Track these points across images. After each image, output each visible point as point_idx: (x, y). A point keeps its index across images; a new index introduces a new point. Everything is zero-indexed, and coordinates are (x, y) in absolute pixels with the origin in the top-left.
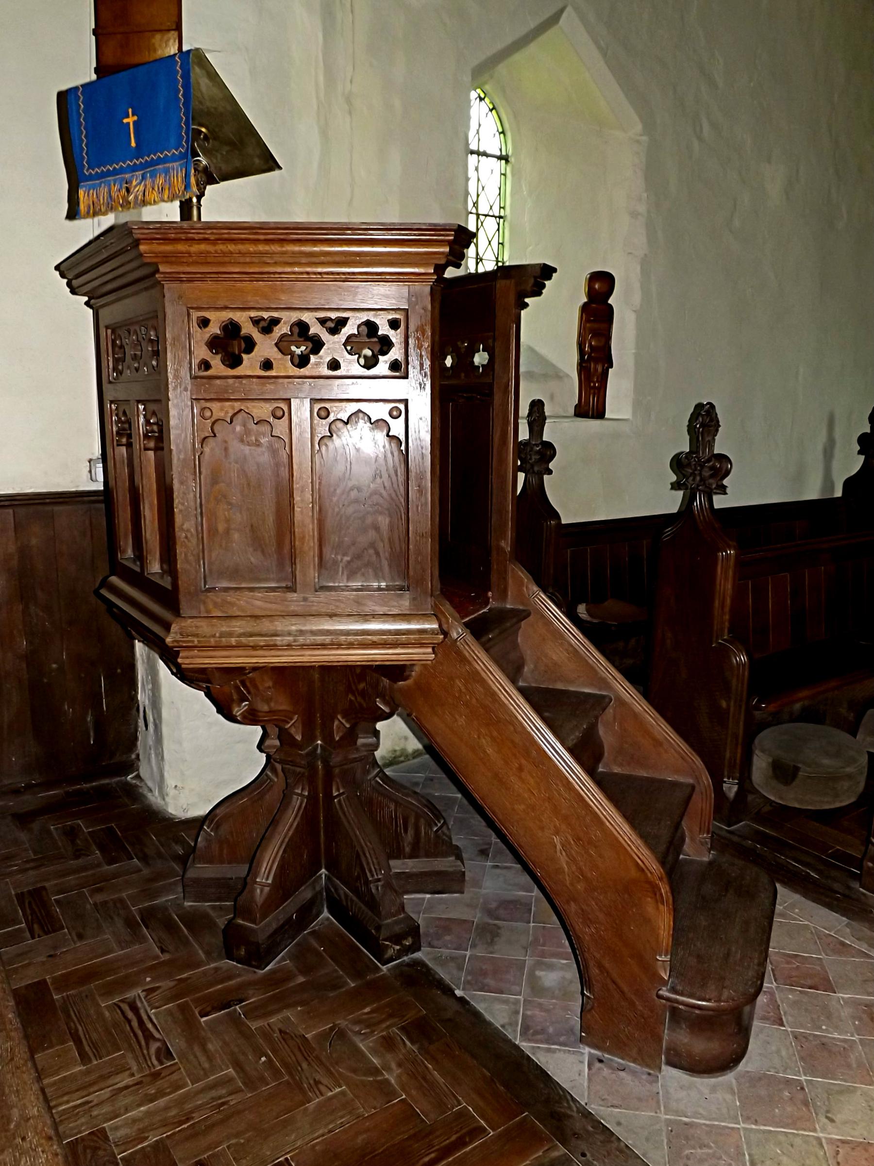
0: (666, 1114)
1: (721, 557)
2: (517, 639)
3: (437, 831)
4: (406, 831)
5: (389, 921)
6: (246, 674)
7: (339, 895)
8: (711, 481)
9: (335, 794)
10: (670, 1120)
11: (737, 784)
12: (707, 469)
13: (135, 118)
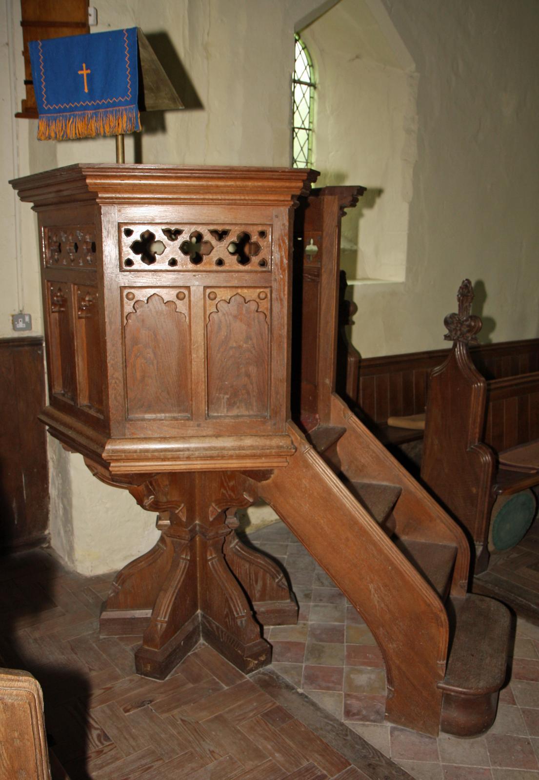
0: (443, 762)
1: (474, 388)
2: (336, 449)
3: (278, 582)
4: (257, 582)
5: (250, 644)
6: (152, 477)
7: (212, 628)
8: (468, 335)
9: (209, 558)
10: (445, 765)
11: (482, 545)
12: (465, 326)
13: (89, 71)
